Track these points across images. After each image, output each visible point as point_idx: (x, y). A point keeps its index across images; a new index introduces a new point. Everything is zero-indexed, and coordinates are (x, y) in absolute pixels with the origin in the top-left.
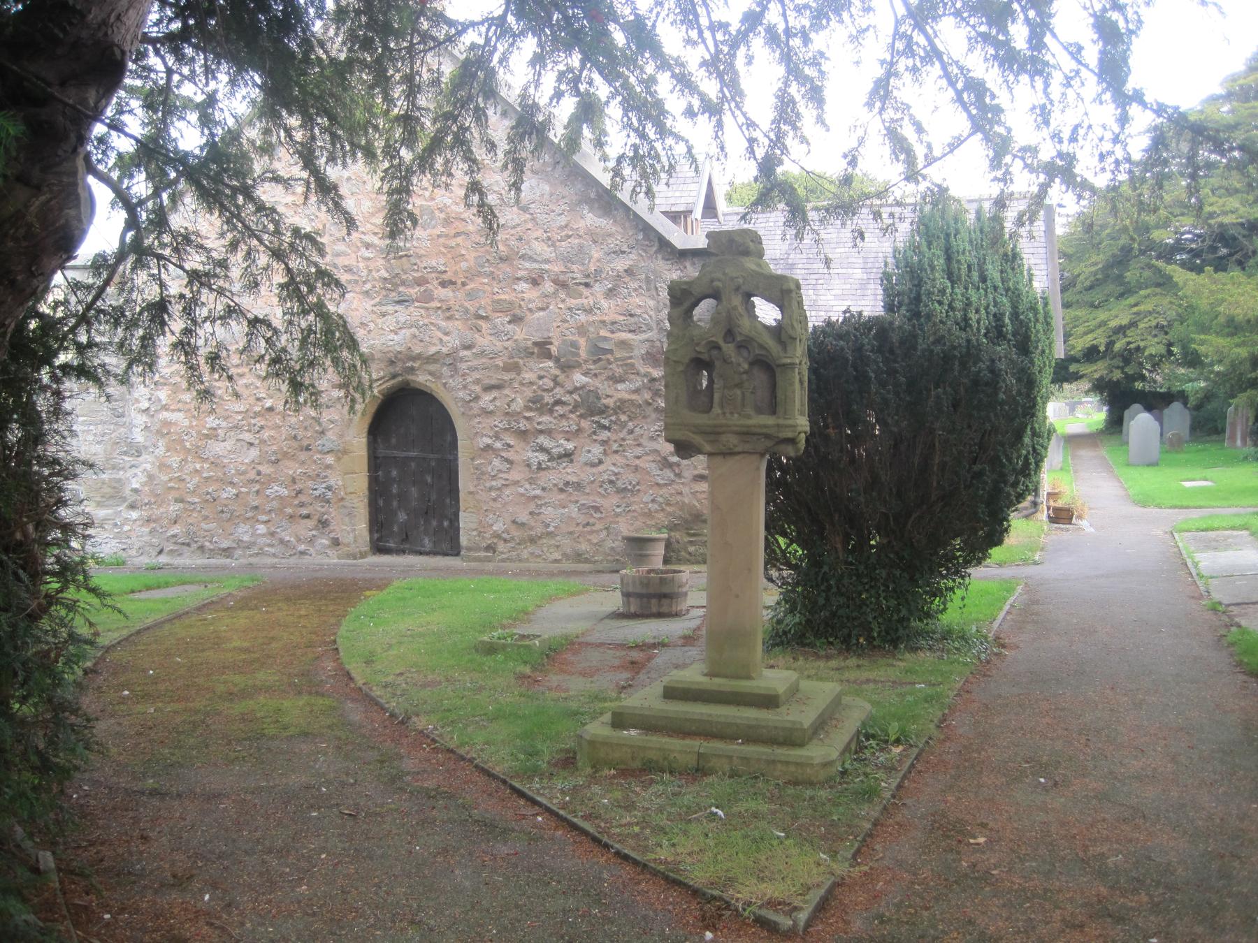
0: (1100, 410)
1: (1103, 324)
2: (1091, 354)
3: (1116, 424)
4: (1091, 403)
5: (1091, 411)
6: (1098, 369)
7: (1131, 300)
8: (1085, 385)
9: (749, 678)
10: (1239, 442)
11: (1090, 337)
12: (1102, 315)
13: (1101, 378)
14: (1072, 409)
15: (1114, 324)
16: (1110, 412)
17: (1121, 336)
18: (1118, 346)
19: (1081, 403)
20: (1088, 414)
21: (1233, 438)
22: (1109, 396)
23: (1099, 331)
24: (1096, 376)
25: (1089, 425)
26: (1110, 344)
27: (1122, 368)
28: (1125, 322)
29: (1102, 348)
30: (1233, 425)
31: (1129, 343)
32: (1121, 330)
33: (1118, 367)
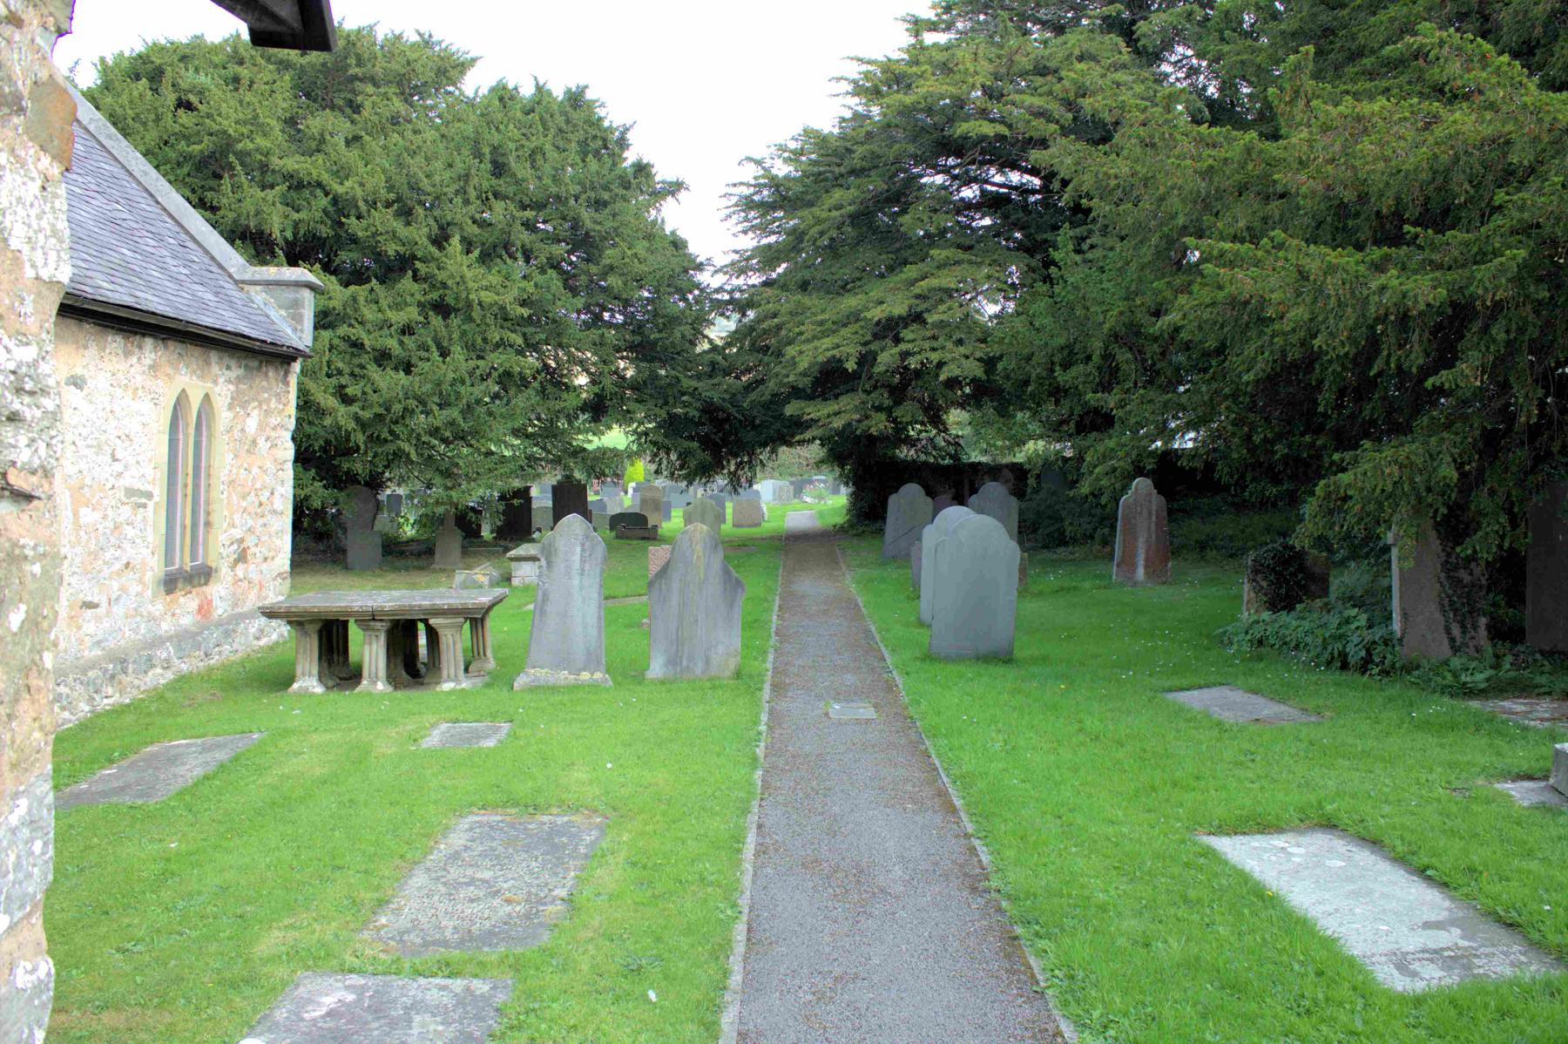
0: (836, 491)
1: (855, 317)
2: (830, 380)
3: (869, 513)
4: (824, 482)
5: (824, 493)
6: (839, 412)
7: (911, 271)
8: (815, 451)
9: (758, 525)
10: (1141, 573)
11: (827, 342)
12: (850, 302)
13: (846, 433)
14: (798, 491)
15: (877, 313)
16: (856, 498)
17: (889, 342)
18: (887, 357)
19: (811, 482)
20: (820, 498)
21: (1128, 563)
22: (854, 471)
23: (845, 332)
24: (838, 423)
25: (821, 514)
26: (867, 360)
27: (889, 411)
28: (899, 309)
29: (851, 366)
30: (1131, 533)
31: (905, 355)
32: (889, 329)
33: (878, 409)
